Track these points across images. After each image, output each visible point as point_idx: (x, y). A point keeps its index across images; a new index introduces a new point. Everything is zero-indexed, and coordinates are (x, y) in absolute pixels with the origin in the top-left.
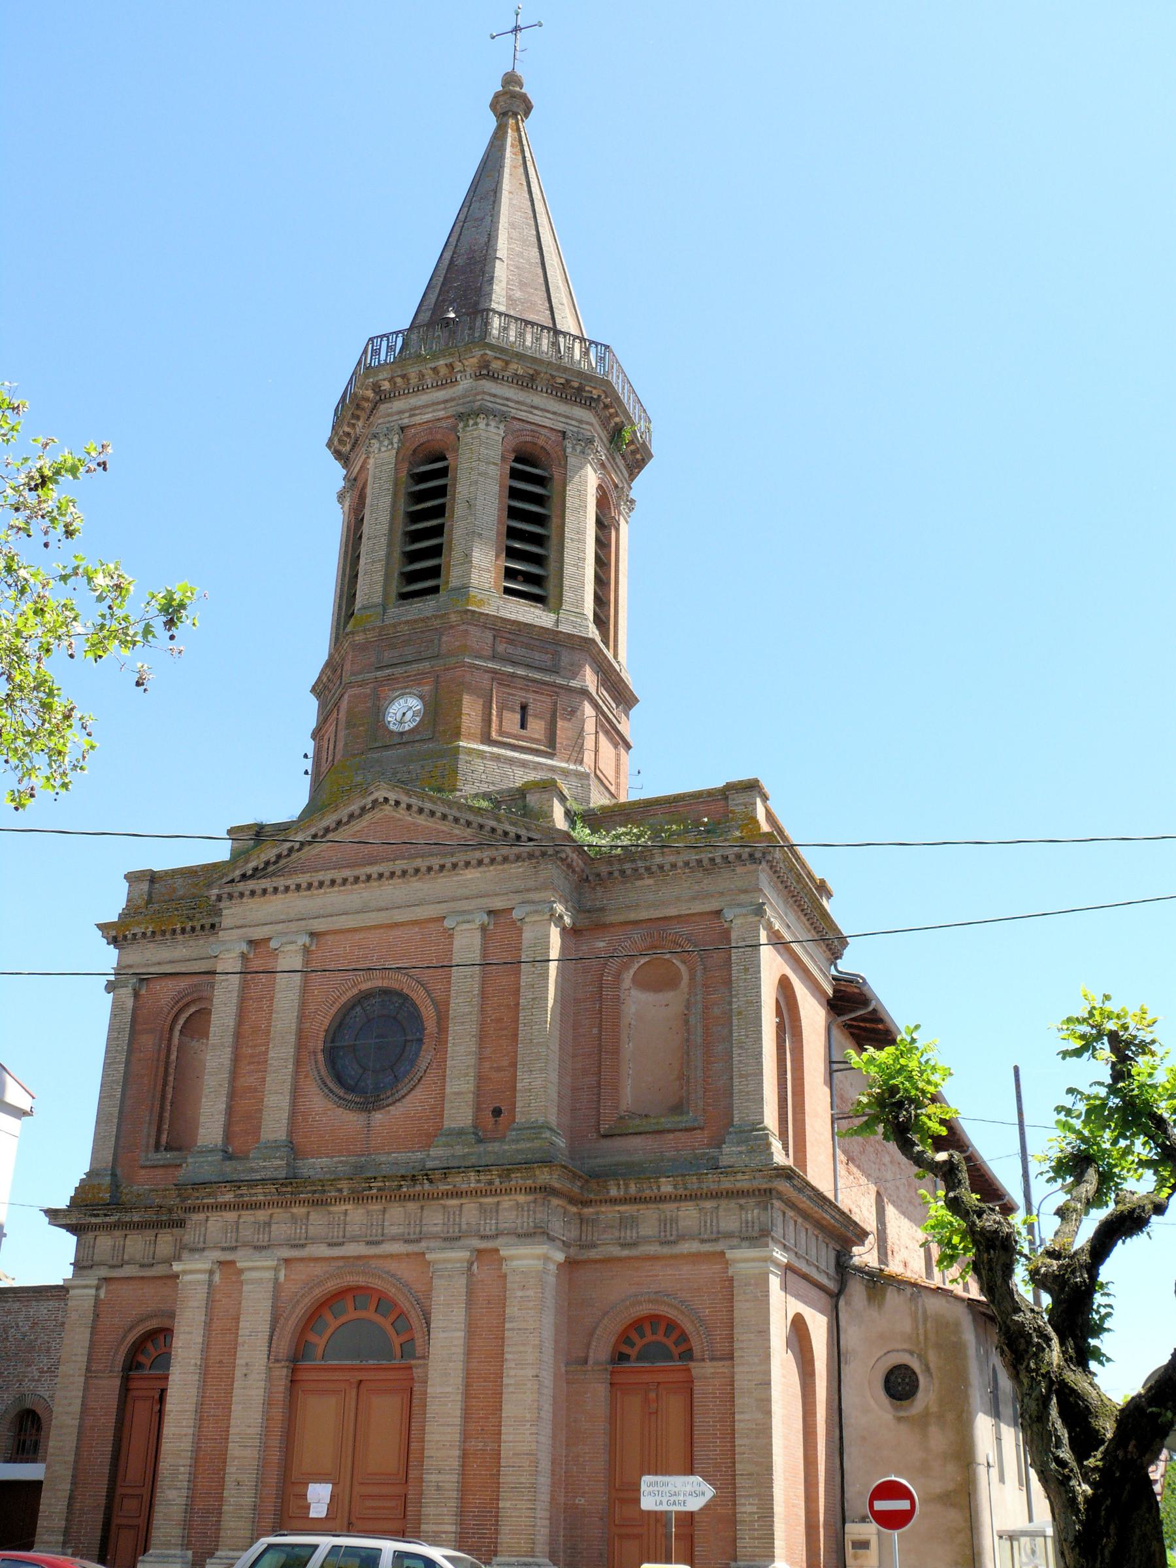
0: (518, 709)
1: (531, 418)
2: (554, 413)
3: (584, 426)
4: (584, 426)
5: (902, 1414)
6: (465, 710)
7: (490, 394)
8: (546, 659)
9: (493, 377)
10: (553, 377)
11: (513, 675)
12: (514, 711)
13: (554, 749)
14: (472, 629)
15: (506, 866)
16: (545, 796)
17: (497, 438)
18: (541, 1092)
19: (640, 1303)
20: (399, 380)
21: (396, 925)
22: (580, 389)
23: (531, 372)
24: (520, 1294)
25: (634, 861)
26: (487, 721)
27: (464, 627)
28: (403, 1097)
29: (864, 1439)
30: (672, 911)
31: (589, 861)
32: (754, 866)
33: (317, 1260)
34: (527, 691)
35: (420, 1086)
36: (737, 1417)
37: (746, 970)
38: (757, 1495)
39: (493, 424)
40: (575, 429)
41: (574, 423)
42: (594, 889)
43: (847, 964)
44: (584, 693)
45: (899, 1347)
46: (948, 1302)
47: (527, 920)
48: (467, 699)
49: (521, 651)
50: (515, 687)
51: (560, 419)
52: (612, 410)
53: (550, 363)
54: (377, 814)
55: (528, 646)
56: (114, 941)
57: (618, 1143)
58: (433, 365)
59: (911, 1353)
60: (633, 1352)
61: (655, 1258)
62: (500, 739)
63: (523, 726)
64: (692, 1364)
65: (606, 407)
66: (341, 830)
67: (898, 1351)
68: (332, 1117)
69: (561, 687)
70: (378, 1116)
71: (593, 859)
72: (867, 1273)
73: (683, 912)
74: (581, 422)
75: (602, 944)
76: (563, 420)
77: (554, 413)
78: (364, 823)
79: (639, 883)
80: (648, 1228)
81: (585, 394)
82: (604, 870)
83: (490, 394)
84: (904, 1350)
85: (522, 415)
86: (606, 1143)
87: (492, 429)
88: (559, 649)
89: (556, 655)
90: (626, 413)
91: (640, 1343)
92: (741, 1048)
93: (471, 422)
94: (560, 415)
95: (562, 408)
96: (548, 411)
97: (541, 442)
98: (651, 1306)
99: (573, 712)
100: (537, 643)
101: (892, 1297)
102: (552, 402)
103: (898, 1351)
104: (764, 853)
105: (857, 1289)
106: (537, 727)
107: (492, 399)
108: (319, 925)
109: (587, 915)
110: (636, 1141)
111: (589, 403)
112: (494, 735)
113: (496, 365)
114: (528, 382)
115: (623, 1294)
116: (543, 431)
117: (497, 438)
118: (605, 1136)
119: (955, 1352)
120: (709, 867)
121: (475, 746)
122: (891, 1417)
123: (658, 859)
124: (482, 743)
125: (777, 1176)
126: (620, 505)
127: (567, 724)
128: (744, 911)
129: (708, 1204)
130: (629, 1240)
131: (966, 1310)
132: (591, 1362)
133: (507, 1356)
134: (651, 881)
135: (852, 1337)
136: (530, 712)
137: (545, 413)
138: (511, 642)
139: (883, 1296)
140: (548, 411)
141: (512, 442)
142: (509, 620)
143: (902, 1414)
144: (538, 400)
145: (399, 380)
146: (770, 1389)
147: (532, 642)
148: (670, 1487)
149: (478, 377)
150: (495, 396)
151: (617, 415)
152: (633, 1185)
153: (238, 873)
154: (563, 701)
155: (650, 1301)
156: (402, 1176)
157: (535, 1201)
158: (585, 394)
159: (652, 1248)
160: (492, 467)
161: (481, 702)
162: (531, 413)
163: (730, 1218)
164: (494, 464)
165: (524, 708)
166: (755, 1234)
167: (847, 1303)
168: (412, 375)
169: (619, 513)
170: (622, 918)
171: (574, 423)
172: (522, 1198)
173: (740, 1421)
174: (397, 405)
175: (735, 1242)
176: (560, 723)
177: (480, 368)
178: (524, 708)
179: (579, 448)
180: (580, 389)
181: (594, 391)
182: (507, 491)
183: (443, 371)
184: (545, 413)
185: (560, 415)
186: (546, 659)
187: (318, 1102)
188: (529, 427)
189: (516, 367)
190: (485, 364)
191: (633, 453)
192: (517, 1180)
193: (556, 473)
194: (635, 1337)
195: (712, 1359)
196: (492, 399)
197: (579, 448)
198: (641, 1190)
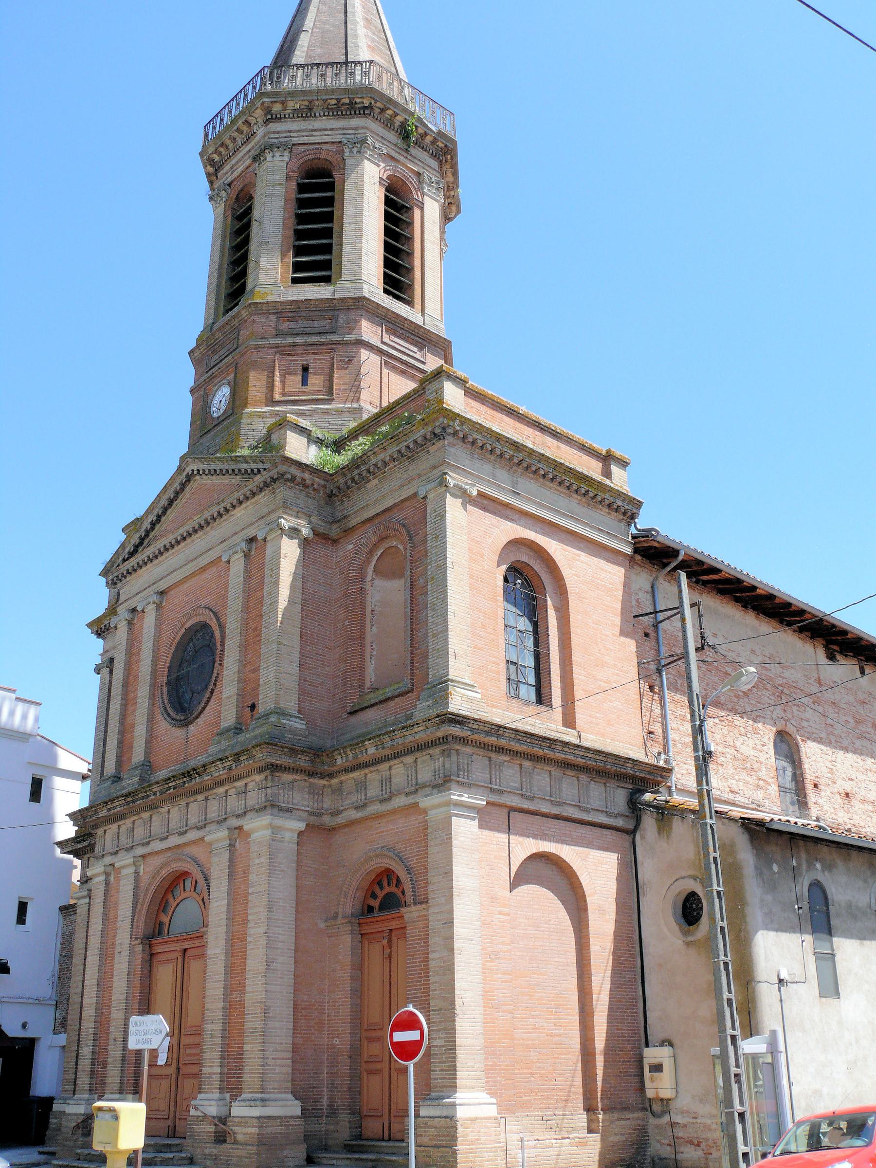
0: (300, 370)
1: (312, 140)
2: (332, 129)
3: (360, 131)
4: (360, 131)
5: (690, 939)
6: (252, 383)
7: (275, 132)
8: (326, 324)
9: (277, 119)
10: (324, 101)
11: (294, 345)
12: (295, 373)
13: (332, 394)
14: (257, 318)
15: (256, 498)
16: (282, 432)
17: (282, 164)
18: (280, 683)
19: (371, 859)
20: (221, 149)
21: (203, 569)
22: (352, 104)
23: (307, 103)
24: (257, 861)
25: (358, 467)
26: (271, 386)
27: (252, 318)
28: (204, 708)
29: (660, 965)
30: (389, 503)
31: (328, 477)
32: (441, 443)
33: (158, 853)
34: (308, 354)
35: (213, 697)
36: (431, 956)
37: (437, 537)
38: (445, 1029)
39: (278, 154)
40: (352, 136)
41: (350, 131)
42: (342, 501)
43: (643, 522)
44: (361, 343)
45: (684, 874)
46: (723, 824)
47: (268, 538)
48: (253, 375)
49: (301, 324)
50: (297, 354)
51: (337, 132)
52: (390, 112)
53: (318, 91)
54: (193, 485)
55: (308, 319)
56: (99, 634)
57: (361, 717)
58: (236, 128)
59: (695, 878)
60: (376, 904)
61: (379, 816)
62: (283, 399)
63: (304, 382)
64: (403, 910)
65: (382, 110)
66: (174, 505)
67: (684, 878)
68: (171, 735)
69: (338, 343)
70: (192, 728)
71: (331, 475)
72: (654, 807)
73: (396, 501)
74: (356, 129)
75: (351, 546)
76: (341, 132)
77: (332, 129)
78: (188, 495)
79: (369, 485)
80: (373, 791)
81: (357, 106)
82: (341, 481)
83: (275, 132)
84: (690, 877)
85: (305, 140)
86: (354, 719)
87: (278, 158)
88: (336, 313)
89: (334, 318)
90: (406, 110)
91: (381, 894)
92: (433, 610)
93: (262, 159)
94: (337, 129)
95: (341, 123)
96: (326, 130)
97: (323, 156)
98: (379, 861)
99: (350, 362)
100: (317, 313)
101: (678, 827)
102: (331, 121)
103: (684, 878)
104: (444, 428)
105: (649, 822)
106: (316, 381)
107: (277, 135)
108: (163, 585)
109: (338, 524)
110: (370, 714)
111: (365, 111)
112: (277, 397)
113: (277, 108)
114: (307, 112)
115: (361, 853)
116: (324, 147)
117: (282, 164)
118: (353, 713)
119: (732, 872)
120: (410, 455)
121: (259, 410)
122: (681, 942)
123: (374, 460)
124: (267, 405)
125: (443, 722)
126: (423, 188)
127: (343, 373)
128: (433, 485)
129: (409, 759)
130: (360, 803)
131: (740, 830)
132: (340, 917)
133: (250, 917)
134: (376, 481)
135: (647, 870)
136: (311, 370)
137: (323, 131)
138: (292, 319)
139: (670, 827)
140: (326, 130)
141: (296, 163)
142: (287, 302)
143: (690, 939)
144: (317, 124)
145: (221, 149)
146: (453, 926)
147: (311, 314)
148: (144, 1027)
149: (267, 122)
150: (278, 132)
151: (396, 114)
152: (349, 753)
153: (121, 559)
154: (341, 353)
155: (377, 856)
156: (183, 774)
157: (266, 778)
158: (357, 106)
159: (376, 807)
160: (278, 187)
161: (265, 373)
162: (312, 135)
163: (427, 767)
164: (280, 184)
165: (305, 369)
166: (440, 781)
167: (643, 838)
168: (228, 142)
169: (423, 194)
170: (358, 520)
171: (350, 131)
172: (258, 778)
173: (433, 960)
174: (227, 168)
175: (428, 790)
176: (336, 374)
177: (265, 115)
178: (305, 369)
179: (355, 150)
180: (352, 104)
181: (365, 101)
182: (294, 203)
183: (245, 129)
184: (323, 131)
185: (337, 129)
186: (326, 324)
187: (163, 725)
188: (312, 147)
189: (292, 104)
190: (268, 111)
191: (433, 142)
192: (245, 764)
193: (337, 177)
194: (377, 890)
195: (415, 904)
196: (277, 135)
197: (355, 150)
198: (355, 757)
